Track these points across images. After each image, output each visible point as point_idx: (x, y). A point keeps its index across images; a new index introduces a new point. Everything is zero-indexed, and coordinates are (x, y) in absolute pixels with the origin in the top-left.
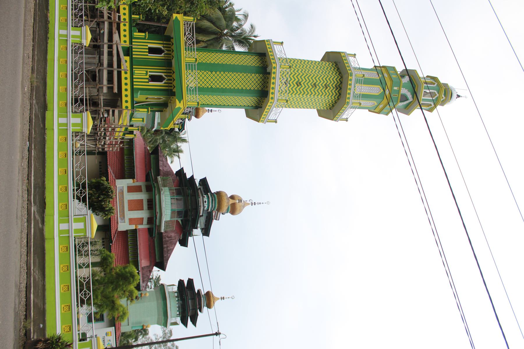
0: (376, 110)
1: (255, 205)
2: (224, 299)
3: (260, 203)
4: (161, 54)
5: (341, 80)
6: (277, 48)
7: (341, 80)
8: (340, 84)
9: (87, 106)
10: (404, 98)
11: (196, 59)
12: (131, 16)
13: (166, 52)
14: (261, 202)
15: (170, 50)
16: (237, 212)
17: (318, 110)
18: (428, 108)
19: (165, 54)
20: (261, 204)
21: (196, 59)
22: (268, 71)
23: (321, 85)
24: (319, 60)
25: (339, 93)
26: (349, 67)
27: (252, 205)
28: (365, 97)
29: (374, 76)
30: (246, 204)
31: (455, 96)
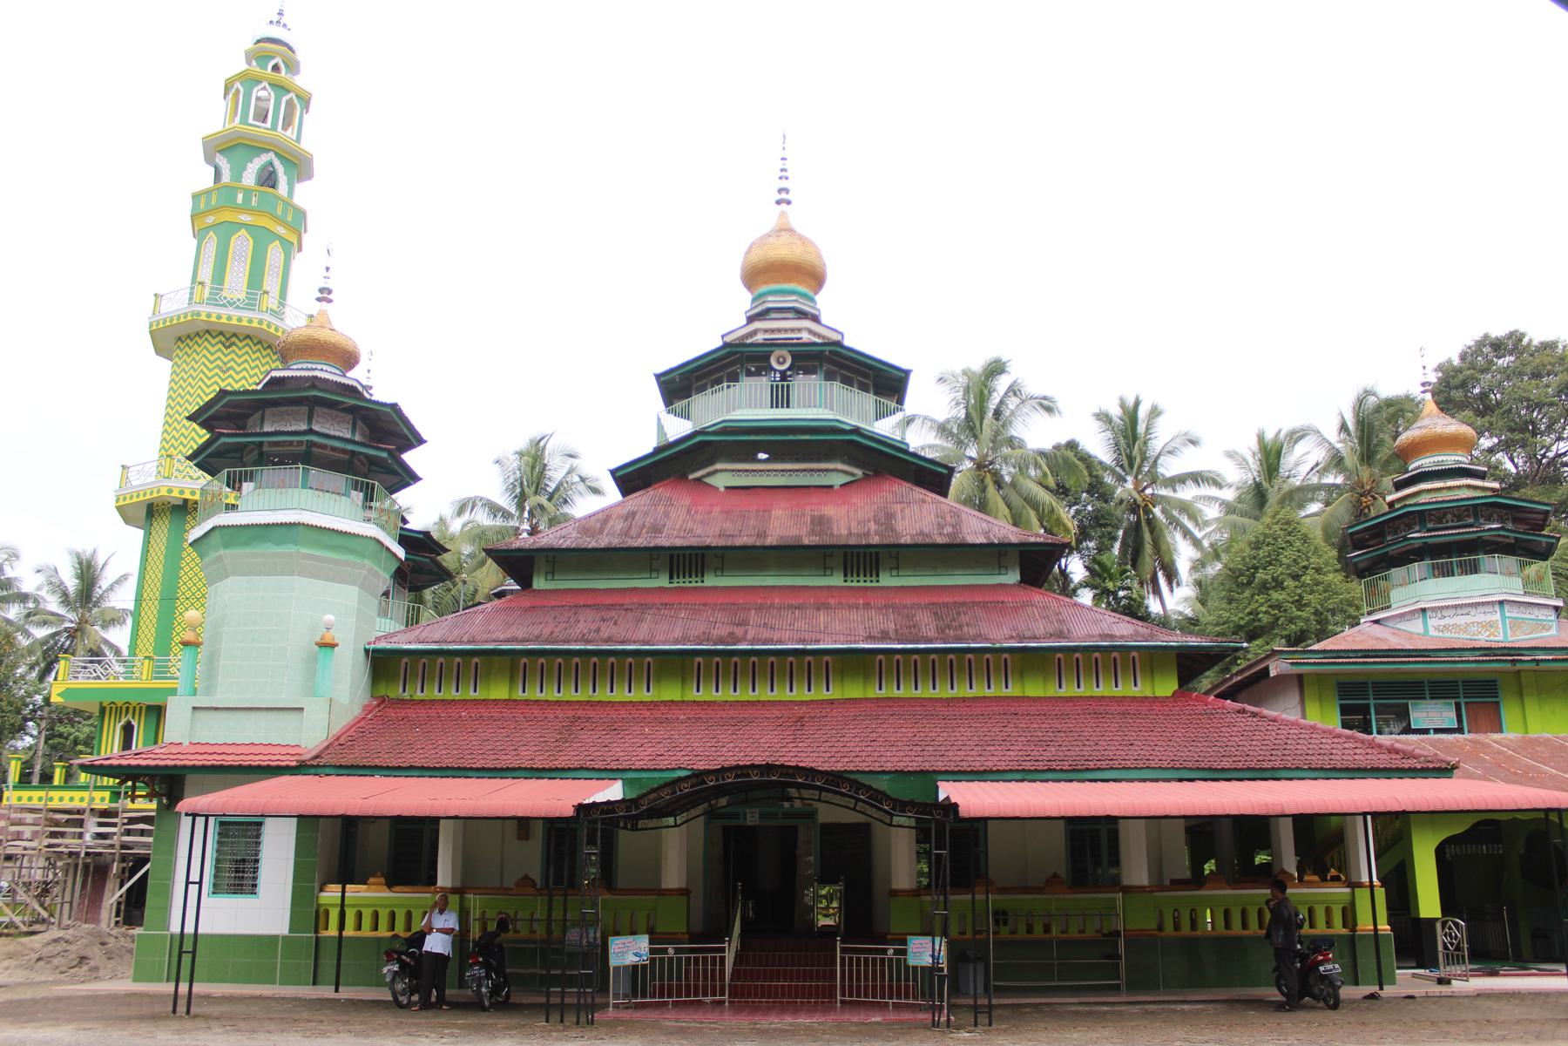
0: (294, 239)
1: (787, 191)
2: (330, 292)
3: (782, 170)
4: (133, 727)
5: (214, 334)
6: (137, 480)
7: (214, 334)
8: (224, 336)
9: (100, 817)
10: (268, 179)
11: (146, 657)
12: (56, 787)
13: (130, 716)
14: (780, 165)
15: (126, 708)
16: (810, 258)
17: (211, 582)
18: (298, 107)
19: (133, 718)
20: (787, 165)
21: (146, 657)
22: (181, 503)
23: (226, 356)
24: (170, 363)
25: (245, 339)
26: (186, 315)
27: (789, 203)
28: (256, 279)
29: (212, 242)
30: (784, 229)
31: (276, 33)
